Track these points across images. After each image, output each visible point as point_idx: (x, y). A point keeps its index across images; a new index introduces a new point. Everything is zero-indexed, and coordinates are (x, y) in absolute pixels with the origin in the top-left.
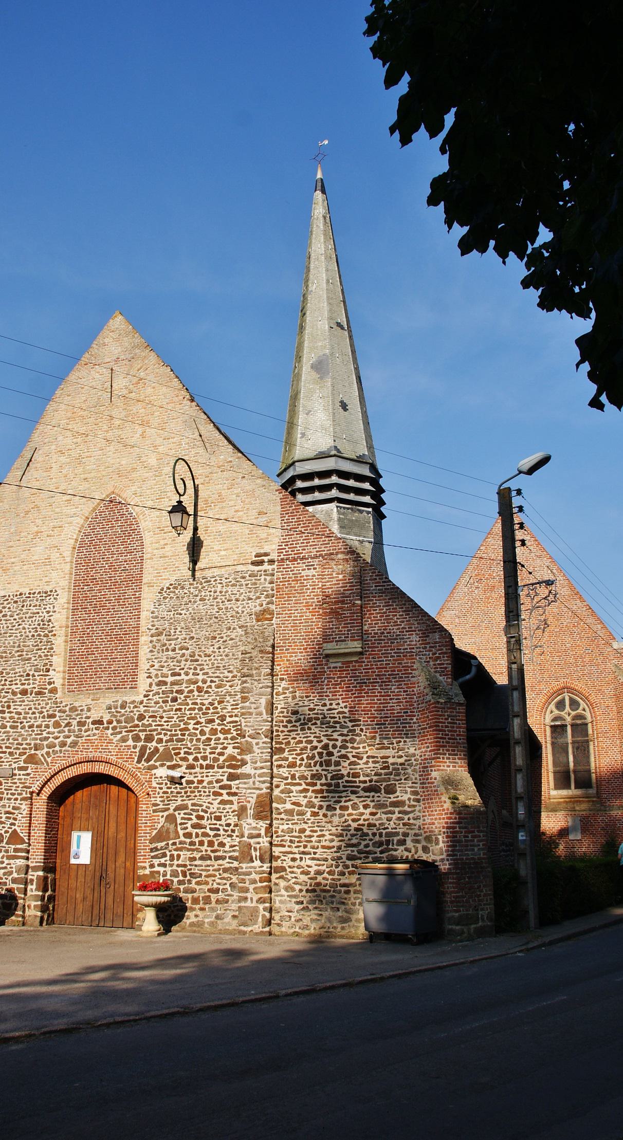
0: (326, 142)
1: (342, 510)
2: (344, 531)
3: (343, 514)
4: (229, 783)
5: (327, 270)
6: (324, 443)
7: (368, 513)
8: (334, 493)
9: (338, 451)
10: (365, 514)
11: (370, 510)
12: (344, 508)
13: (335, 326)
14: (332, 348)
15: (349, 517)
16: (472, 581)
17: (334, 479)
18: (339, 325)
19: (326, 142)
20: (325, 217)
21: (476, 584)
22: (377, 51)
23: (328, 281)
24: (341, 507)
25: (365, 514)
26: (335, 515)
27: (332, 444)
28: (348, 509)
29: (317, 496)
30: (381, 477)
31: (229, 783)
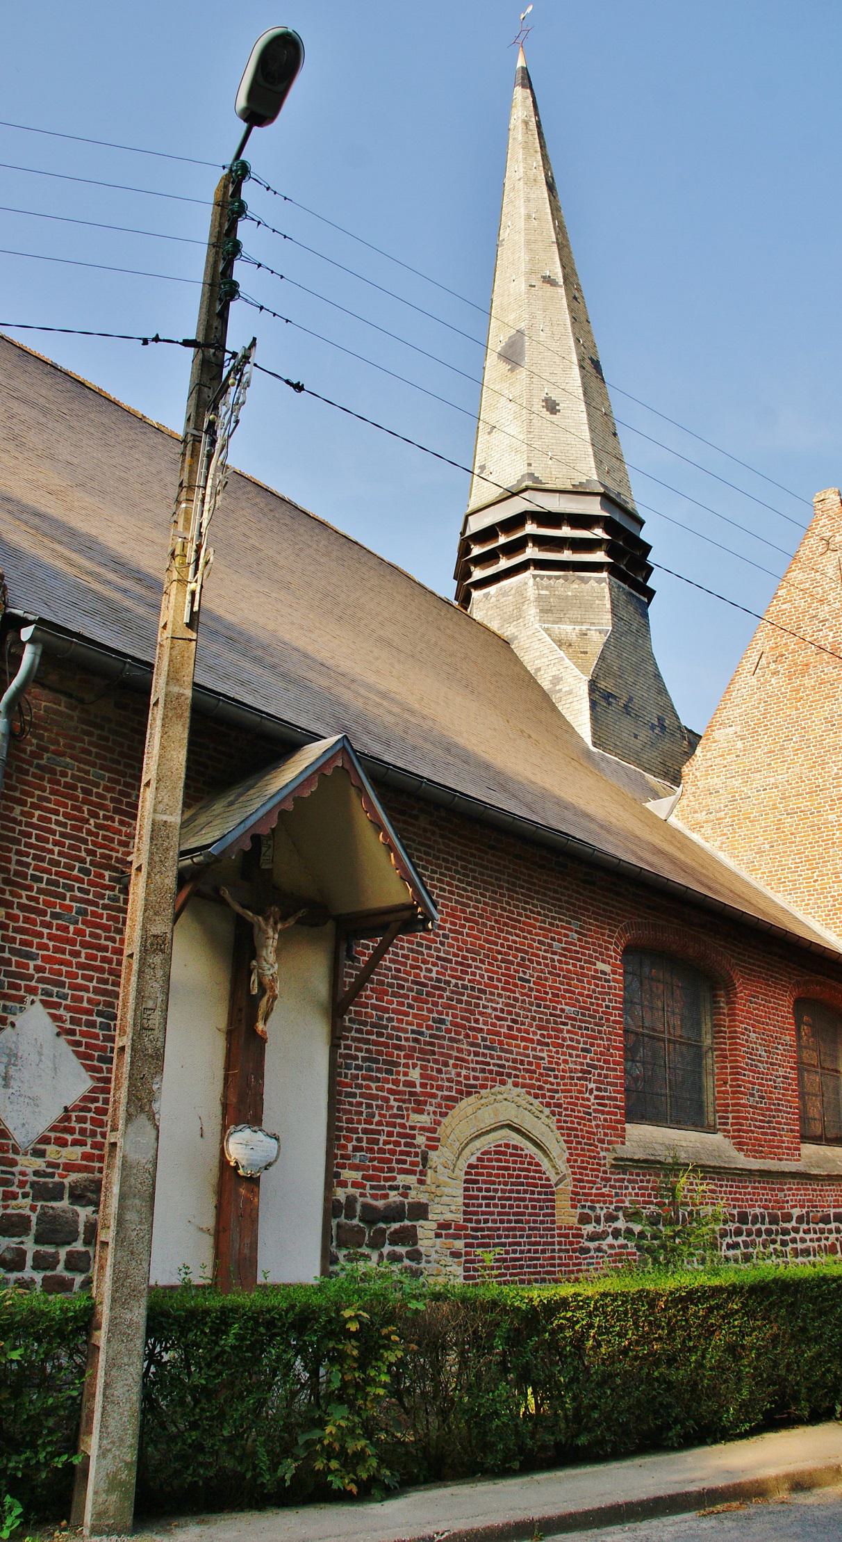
0: (530, 9)
1: (545, 582)
2: (550, 617)
3: (547, 588)
4: (68, 1275)
5: (528, 200)
6: (511, 475)
7: (600, 581)
8: (531, 552)
9: (536, 480)
10: (592, 583)
11: (605, 575)
12: (550, 578)
13: (538, 283)
14: (533, 316)
15: (560, 591)
16: (763, 661)
17: (530, 528)
18: (548, 280)
19: (530, 9)
20: (526, 123)
21: (773, 666)
22: (647, 548)
23: (528, 217)
24: (542, 577)
25: (592, 583)
26: (531, 592)
27: (525, 470)
28: (558, 578)
29: (504, 563)
30: (641, 523)
31: (68, 1275)
